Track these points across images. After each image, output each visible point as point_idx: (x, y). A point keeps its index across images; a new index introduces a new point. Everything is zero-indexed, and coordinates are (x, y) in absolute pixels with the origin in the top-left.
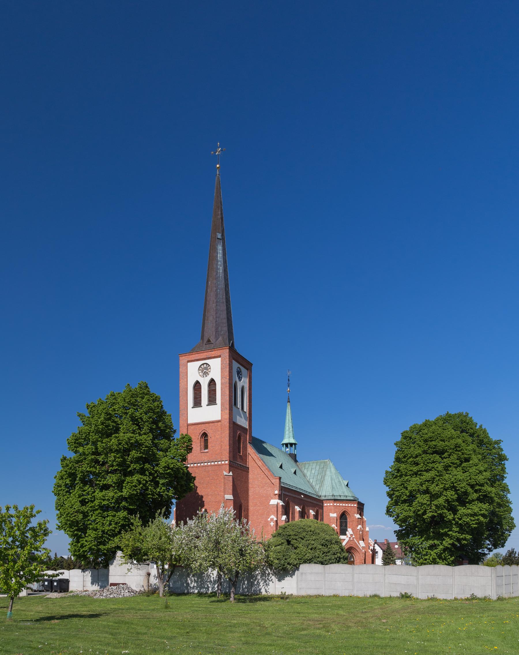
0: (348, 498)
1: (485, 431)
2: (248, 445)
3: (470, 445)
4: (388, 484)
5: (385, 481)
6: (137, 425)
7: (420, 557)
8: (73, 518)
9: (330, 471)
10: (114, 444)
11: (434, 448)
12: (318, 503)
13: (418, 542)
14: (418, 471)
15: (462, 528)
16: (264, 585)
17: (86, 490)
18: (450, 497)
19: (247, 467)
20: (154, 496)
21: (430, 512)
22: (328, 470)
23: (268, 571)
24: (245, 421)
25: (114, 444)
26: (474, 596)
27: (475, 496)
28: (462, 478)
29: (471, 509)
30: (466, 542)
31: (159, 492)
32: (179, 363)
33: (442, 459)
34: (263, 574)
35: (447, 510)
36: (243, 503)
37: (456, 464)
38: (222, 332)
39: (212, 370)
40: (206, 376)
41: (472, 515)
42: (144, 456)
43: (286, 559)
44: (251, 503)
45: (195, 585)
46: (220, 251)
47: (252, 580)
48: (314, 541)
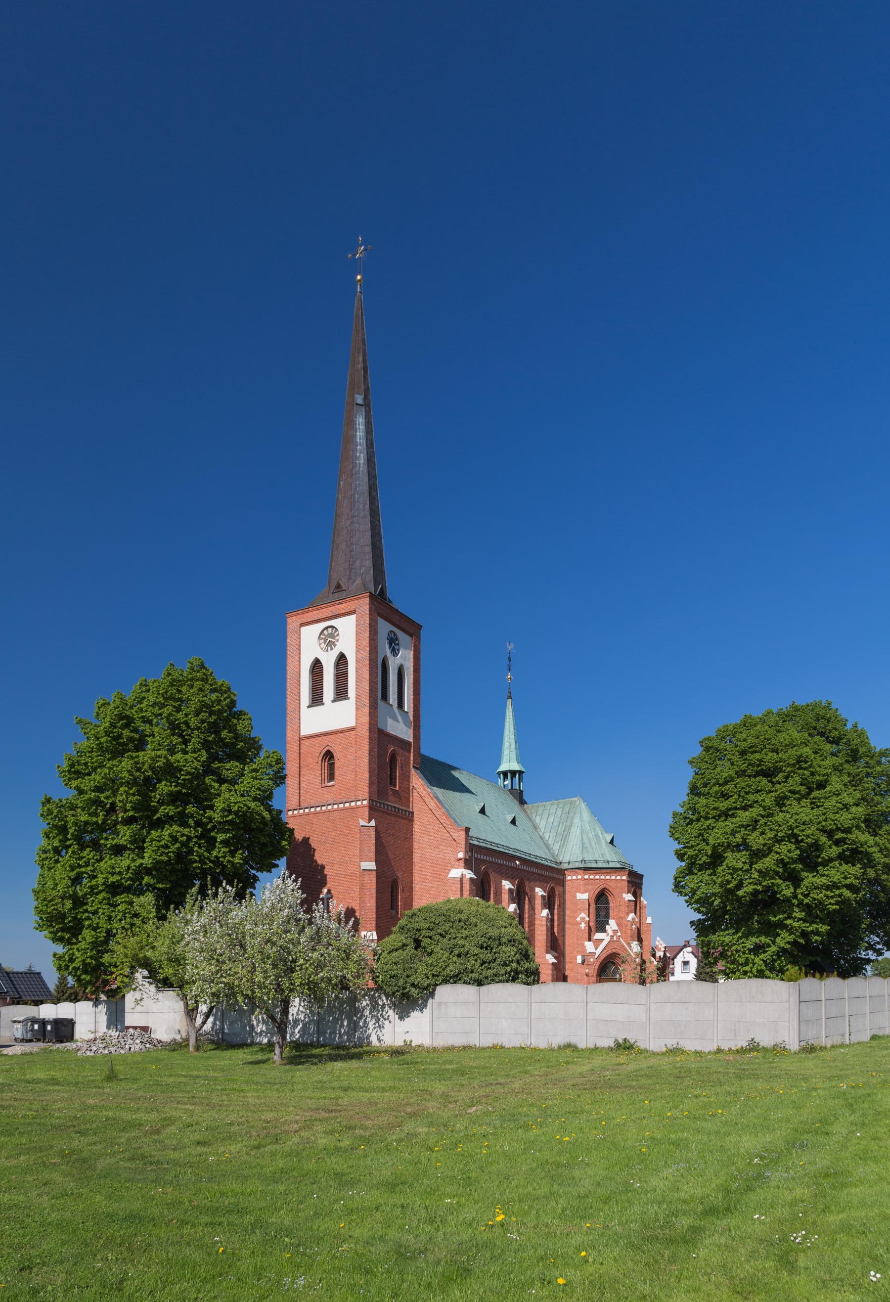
0: (611, 865)
1: (861, 735)
2: (413, 771)
3: (828, 758)
4: (677, 835)
5: (672, 830)
6: (181, 736)
7: (735, 968)
8: (53, 908)
9: (581, 817)
10: (124, 769)
11: (758, 766)
12: (554, 875)
13: (730, 940)
14: (729, 809)
15: (812, 912)
16: (375, 1028)
17: (84, 857)
18: (786, 856)
19: (409, 812)
20: (205, 864)
21: (750, 883)
22: (578, 816)
23: (383, 1000)
24: (405, 728)
25: (124, 769)
26: (756, 1044)
27: (835, 851)
28: (807, 819)
29: (827, 876)
30: (819, 938)
31: (216, 857)
32: (286, 629)
33: (773, 783)
34: (374, 1006)
35: (781, 878)
36: (400, 877)
37: (798, 792)
38: (363, 570)
39: (341, 638)
40: (332, 649)
41: (828, 888)
42: (184, 791)
43: (408, 976)
44: (416, 877)
45: (264, 1029)
46: (361, 427)
47: (355, 1018)
48: (466, 939)
